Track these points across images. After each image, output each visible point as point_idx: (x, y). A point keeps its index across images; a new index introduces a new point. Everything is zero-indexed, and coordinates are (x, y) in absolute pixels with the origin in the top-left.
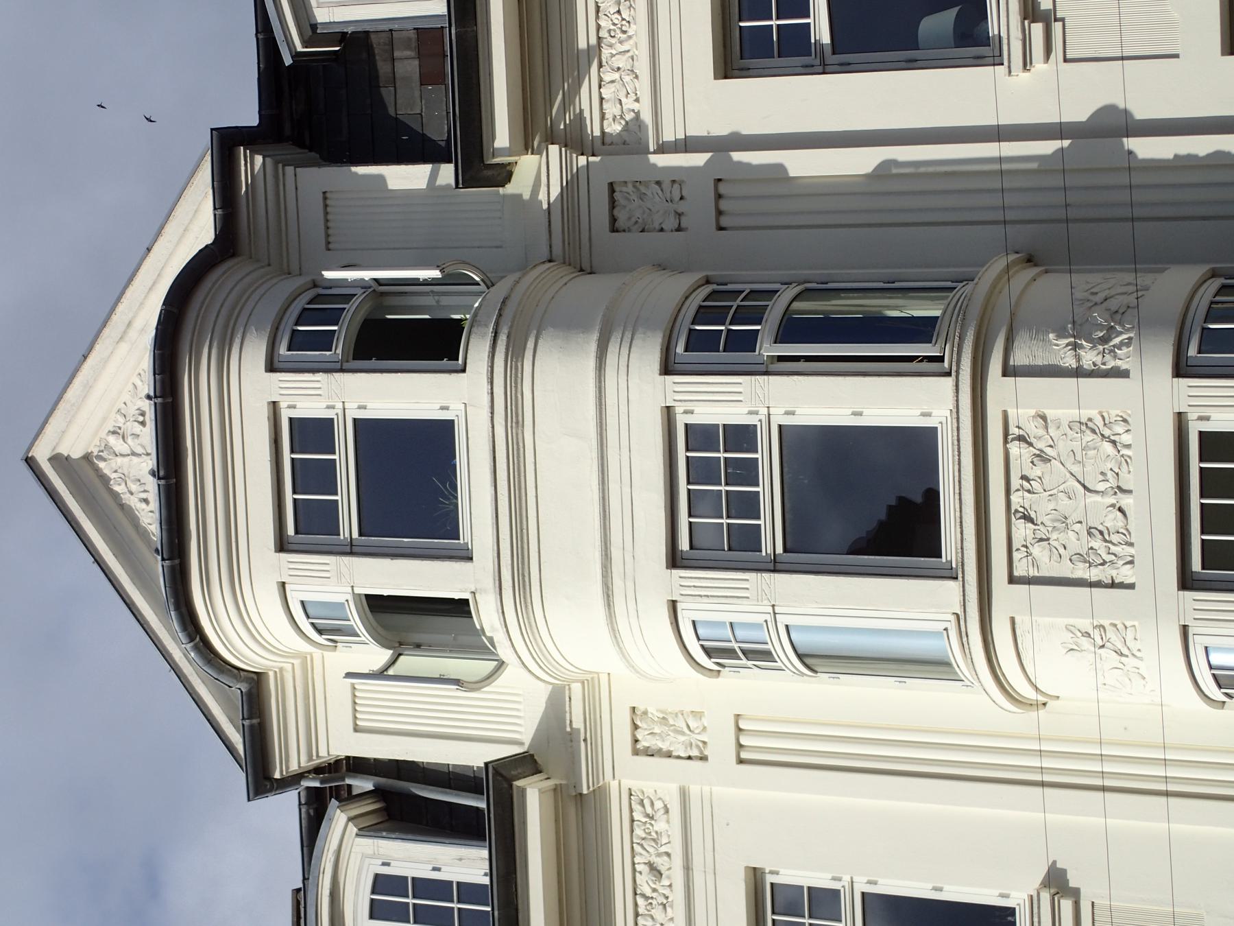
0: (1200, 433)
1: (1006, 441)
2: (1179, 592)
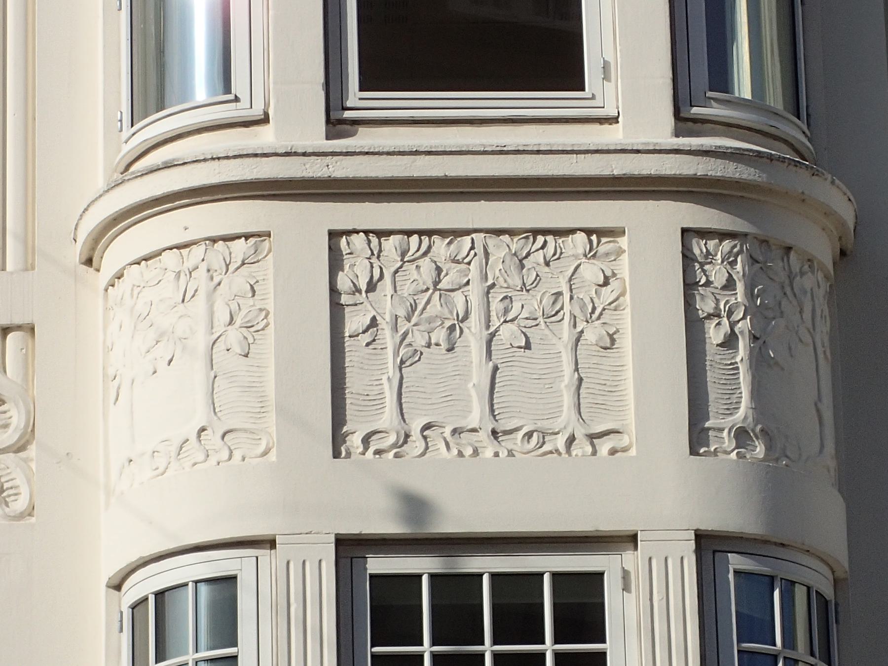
0: (601, 575)
1: (589, 232)
2: (333, 536)
